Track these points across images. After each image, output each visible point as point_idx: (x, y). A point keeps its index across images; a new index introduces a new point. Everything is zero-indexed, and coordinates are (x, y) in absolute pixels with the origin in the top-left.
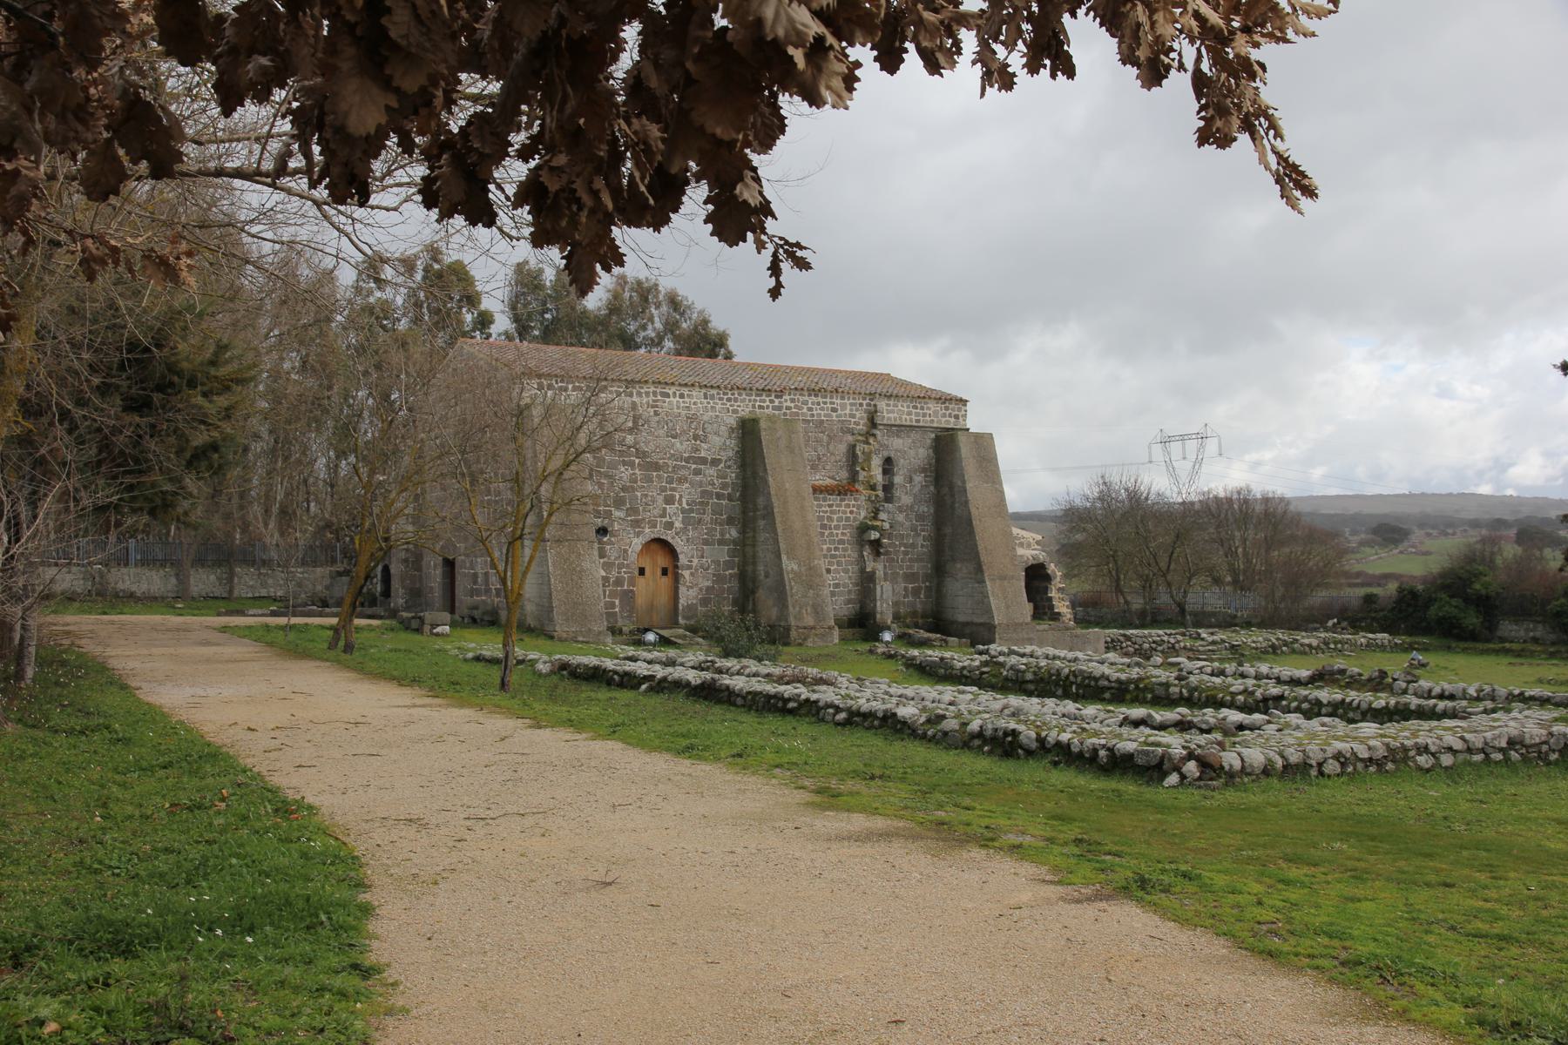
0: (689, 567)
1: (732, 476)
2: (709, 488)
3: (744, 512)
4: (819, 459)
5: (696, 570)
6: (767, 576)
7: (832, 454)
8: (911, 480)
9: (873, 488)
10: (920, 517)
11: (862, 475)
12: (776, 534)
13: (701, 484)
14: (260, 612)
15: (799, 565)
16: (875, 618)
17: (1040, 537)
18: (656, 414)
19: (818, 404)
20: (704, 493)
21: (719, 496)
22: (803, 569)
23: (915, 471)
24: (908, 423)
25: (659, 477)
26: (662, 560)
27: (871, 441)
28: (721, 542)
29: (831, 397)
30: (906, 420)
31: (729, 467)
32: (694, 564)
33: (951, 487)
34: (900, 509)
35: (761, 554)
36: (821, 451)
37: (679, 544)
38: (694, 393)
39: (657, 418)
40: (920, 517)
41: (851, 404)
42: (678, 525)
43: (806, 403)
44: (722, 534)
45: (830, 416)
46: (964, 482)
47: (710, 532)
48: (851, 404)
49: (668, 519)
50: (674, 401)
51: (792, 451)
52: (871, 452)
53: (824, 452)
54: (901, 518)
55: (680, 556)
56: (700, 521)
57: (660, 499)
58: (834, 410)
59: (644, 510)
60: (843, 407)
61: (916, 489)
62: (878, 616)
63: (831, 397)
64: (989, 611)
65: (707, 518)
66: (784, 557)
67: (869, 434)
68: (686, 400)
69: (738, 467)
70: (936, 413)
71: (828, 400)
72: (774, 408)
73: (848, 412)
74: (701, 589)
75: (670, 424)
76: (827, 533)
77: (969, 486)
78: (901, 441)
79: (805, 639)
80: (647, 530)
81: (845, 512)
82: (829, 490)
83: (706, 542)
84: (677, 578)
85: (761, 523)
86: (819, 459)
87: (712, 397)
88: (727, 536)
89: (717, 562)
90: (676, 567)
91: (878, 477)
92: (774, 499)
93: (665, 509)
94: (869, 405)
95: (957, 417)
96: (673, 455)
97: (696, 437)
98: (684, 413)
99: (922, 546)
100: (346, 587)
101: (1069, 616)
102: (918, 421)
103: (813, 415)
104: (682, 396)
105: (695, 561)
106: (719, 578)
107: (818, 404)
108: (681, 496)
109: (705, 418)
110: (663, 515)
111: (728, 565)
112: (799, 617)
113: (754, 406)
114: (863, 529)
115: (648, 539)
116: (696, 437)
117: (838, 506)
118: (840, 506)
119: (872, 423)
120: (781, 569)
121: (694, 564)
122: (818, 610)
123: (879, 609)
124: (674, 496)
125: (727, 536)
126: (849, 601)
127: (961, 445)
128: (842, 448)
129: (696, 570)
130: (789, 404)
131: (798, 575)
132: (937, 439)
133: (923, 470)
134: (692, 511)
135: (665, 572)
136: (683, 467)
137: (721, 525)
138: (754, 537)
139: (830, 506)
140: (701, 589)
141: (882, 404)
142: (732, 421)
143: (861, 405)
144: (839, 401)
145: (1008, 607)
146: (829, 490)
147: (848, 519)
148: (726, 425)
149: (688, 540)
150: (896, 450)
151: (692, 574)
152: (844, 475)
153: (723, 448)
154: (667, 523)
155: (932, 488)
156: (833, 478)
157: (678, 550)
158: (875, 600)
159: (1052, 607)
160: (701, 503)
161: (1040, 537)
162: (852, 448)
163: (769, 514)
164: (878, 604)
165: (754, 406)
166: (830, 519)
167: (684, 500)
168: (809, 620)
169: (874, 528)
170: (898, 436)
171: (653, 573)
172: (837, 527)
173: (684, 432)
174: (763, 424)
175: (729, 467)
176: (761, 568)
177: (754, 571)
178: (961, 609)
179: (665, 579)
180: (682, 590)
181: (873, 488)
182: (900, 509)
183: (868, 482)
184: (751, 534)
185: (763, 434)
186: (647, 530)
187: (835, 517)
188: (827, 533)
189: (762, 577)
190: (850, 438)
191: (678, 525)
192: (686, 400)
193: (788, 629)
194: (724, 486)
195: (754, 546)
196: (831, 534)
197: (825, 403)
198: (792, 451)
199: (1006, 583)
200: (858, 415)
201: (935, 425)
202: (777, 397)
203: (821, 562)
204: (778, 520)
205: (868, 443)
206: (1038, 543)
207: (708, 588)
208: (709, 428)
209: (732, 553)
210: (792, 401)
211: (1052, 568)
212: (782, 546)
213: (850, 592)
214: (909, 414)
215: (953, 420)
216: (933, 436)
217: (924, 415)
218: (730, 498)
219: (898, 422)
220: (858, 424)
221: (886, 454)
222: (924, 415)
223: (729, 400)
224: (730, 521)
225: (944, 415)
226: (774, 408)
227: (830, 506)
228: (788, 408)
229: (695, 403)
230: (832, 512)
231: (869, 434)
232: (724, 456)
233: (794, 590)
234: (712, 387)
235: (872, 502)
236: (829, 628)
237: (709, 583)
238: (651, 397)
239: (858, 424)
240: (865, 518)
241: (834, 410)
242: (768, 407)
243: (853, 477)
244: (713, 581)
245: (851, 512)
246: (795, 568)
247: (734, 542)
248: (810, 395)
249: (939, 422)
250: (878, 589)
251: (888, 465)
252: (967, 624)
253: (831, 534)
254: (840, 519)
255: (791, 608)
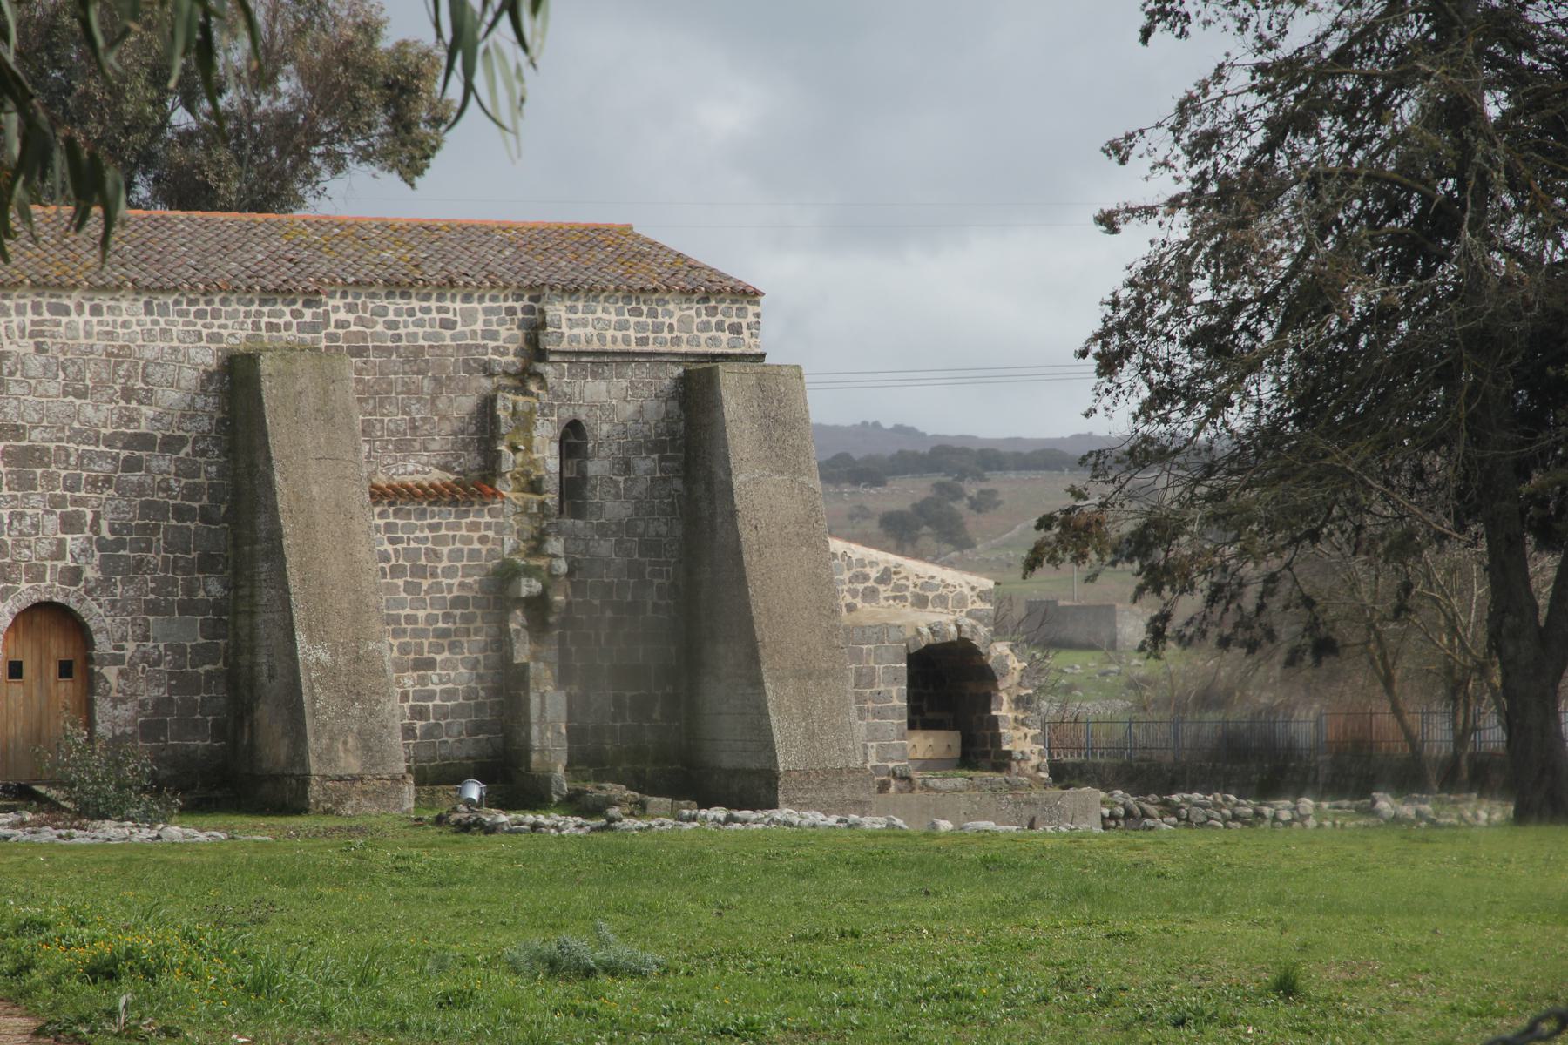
0: (116, 660)
1: (210, 470)
2: (160, 497)
3: (236, 546)
4: (414, 428)
5: (133, 666)
6: (271, 677)
7: (443, 417)
8: (627, 467)
9: (534, 486)
10: (650, 547)
11: (509, 462)
12: (287, 591)
13: (140, 489)
14: (441, 80)
15: (334, 652)
16: (528, 762)
17: (990, 584)
18: (39, 348)
19: (411, 313)
20: (147, 507)
21: (180, 513)
22: (342, 660)
23: (638, 449)
24: (620, 347)
25: (50, 478)
26: (59, 648)
27: (533, 387)
28: (187, 608)
29: (441, 298)
30: (614, 340)
31: (203, 453)
32: (128, 654)
33: (710, 485)
34: (603, 531)
35: (262, 631)
36: (418, 411)
37: (95, 613)
38: (124, 305)
39: (42, 358)
40: (650, 547)
41: (487, 311)
42: (90, 573)
43: (383, 312)
44: (190, 590)
45: (437, 337)
46: (729, 472)
47: (163, 586)
48: (487, 311)
49: (69, 561)
50: (80, 321)
51: (330, 419)
52: (532, 411)
53: (425, 412)
54: (604, 548)
55: (98, 638)
56: (139, 565)
57: (52, 523)
58: (447, 324)
59: (16, 545)
60: (469, 317)
61: (641, 487)
62: (535, 757)
63: (441, 298)
64: (768, 746)
65: (155, 558)
66: (301, 638)
67: (524, 377)
68: (106, 317)
69: (224, 453)
70: (685, 323)
71: (433, 304)
72: (302, 328)
73: (479, 326)
74: (142, 705)
75: (72, 370)
76: (425, 584)
77: (738, 480)
78: (603, 386)
79: (339, 802)
80: (23, 586)
81: (469, 541)
82: (433, 495)
83: (153, 608)
84: (90, 683)
85: (264, 567)
86: (414, 428)
87: (164, 310)
88: (201, 594)
89: (178, 650)
90: (89, 659)
91: (548, 456)
92: (285, 521)
93: (62, 543)
94: (526, 310)
95: (736, 329)
96: (78, 432)
97: (128, 394)
98: (100, 345)
99: (656, 607)
100: (719, 510)
101: (1035, 760)
102: (642, 341)
103: (398, 338)
104: (96, 311)
105: (130, 647)
106: (183, 681)
107: (411, 313)
108: (97, 516)
109: (147, 354)
110: (59, 554)
111: (202, 654)
112: (328, 756)
113: (256, 326)
114: (505, 575)
115: (25, 603)
116: (128, 394)
117: (449, 527)
118: (458, 526)
119: (535, 350)
120: (295, 660)
121: (128, 654)
122: (369, 744)
123: (536, 743)
124: (81, 516)
125: (201, 594)
126: (477, 728)
127: (725, 394)
128: (468, 403)
129: (133, 666)
130: (342, 315)
131: (326, 671)
132: (685, 380)
133: (657, 446)
134: (120, 544)
135: (65, 670)
136: (101, 455)
137: (186, 571)
138: (252, 596)
139: (434, 528)
140: (142, 705)
141: (557, 310)
142: (207, 358)
143: (511, 311)
144: (458, 305)
145: (810, 736)
146: (433, 495)
147: (474, 554)
148: (195, 367)
149: (113, 604)
150: (591, 406)
151: (122, 674)
152: (472, 459)
153: (190, 413)
154: (67, 569)
155: (678, 484)
156: (445, 467)
157: (93, 625)
158: (527, 724)
159: (997, 739)
160: (143, 529)
161: (990, 584)
162: (487, 405)
163: (276, 553)
164: (535, 731)
165: (256, 326)
166: (437, 556)
167: (104, 524)
168: (351, 764)
169: (530, 572)
170: (595, 375)
171: (41, 673)
172: (450, 571)
173: (100, 384)
174: (266, 365)
175: (203, 453)
176: (262, 659)
177: (252, 667)
178: (728, 753)
179: (65, 686)
180: (102, 706)
181: (534, 486)
182: (603, 531)
183: (527, 474)
184: (244, 592)
185: (266, 385)
186: (23, 586)
187: (445, 550)
188: (425, 584)
189: (264, 679)
190: (487, 384)
191: (90, 573)
192: (106, 317)
193: (304, 781)
194: (192, 492)
195: (252, 614)
196: (437, 587)
197: (427, 311)
198: (330, 419)
199: (810, 685)
200: (504, 332)
201: (684, 348)
202: (307, 304)
203: (384, 647)
204: (292, 561)
205: (527, 393)
206: (983, 596)
207: (158, 703)
208: (157, 374)
209: (211, 630)
210: (351, 308)
211: (1000, 652)
212: (298, 615)
213: (479, 707)
214: (623, 326)
215: (726, 336)
216: (679, 371)
217: (658, 328)
218: (206, 516)
219: (596, 346)
220: (504, 353)
221: (567, 414)
222: (658, 328)
223: (200, 314)
224: (207, 564)
225: (705, 327)
226: (302, 328)
227: (434, 528)
228: (341, 324)
229: (125, 325)
230: (437, 541)
231: (524, 377)
232: (190, 430)
233: (319, 701)
234: (162, 290)
235: (531, 516)
236: (394, 779)
237: (161, 692)
238: (30, 316)
239: (504, 353)
240: (516, 551)
241: (447, 324)
242: (288, 326)
243: (490, 468)
244: (171, 689)
245: (483, 540)
246: (325, 657)
247: (217, 606)
248: (389, 295)
249: (693, 340)
250: (534, 700)
251: (573, 438)
252: (734, 773)
253: (437, 587)
254: (456, 555)
255: (311, 740)
